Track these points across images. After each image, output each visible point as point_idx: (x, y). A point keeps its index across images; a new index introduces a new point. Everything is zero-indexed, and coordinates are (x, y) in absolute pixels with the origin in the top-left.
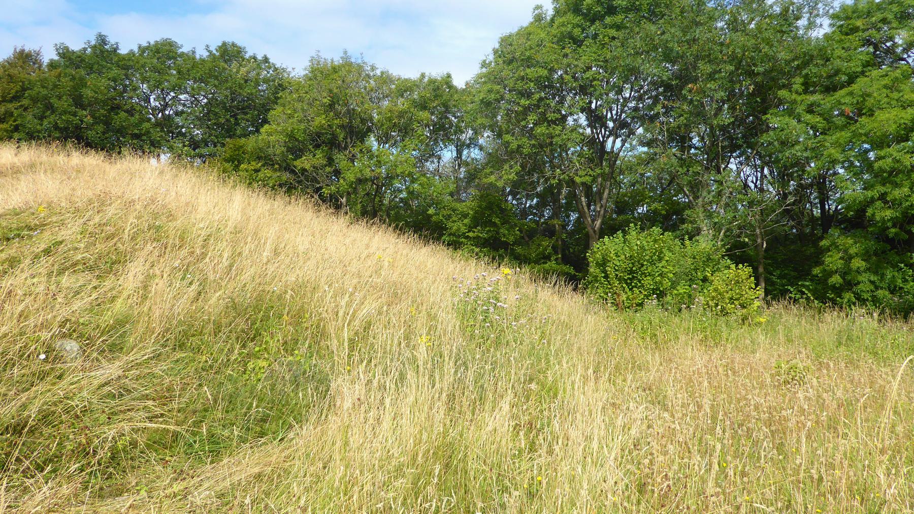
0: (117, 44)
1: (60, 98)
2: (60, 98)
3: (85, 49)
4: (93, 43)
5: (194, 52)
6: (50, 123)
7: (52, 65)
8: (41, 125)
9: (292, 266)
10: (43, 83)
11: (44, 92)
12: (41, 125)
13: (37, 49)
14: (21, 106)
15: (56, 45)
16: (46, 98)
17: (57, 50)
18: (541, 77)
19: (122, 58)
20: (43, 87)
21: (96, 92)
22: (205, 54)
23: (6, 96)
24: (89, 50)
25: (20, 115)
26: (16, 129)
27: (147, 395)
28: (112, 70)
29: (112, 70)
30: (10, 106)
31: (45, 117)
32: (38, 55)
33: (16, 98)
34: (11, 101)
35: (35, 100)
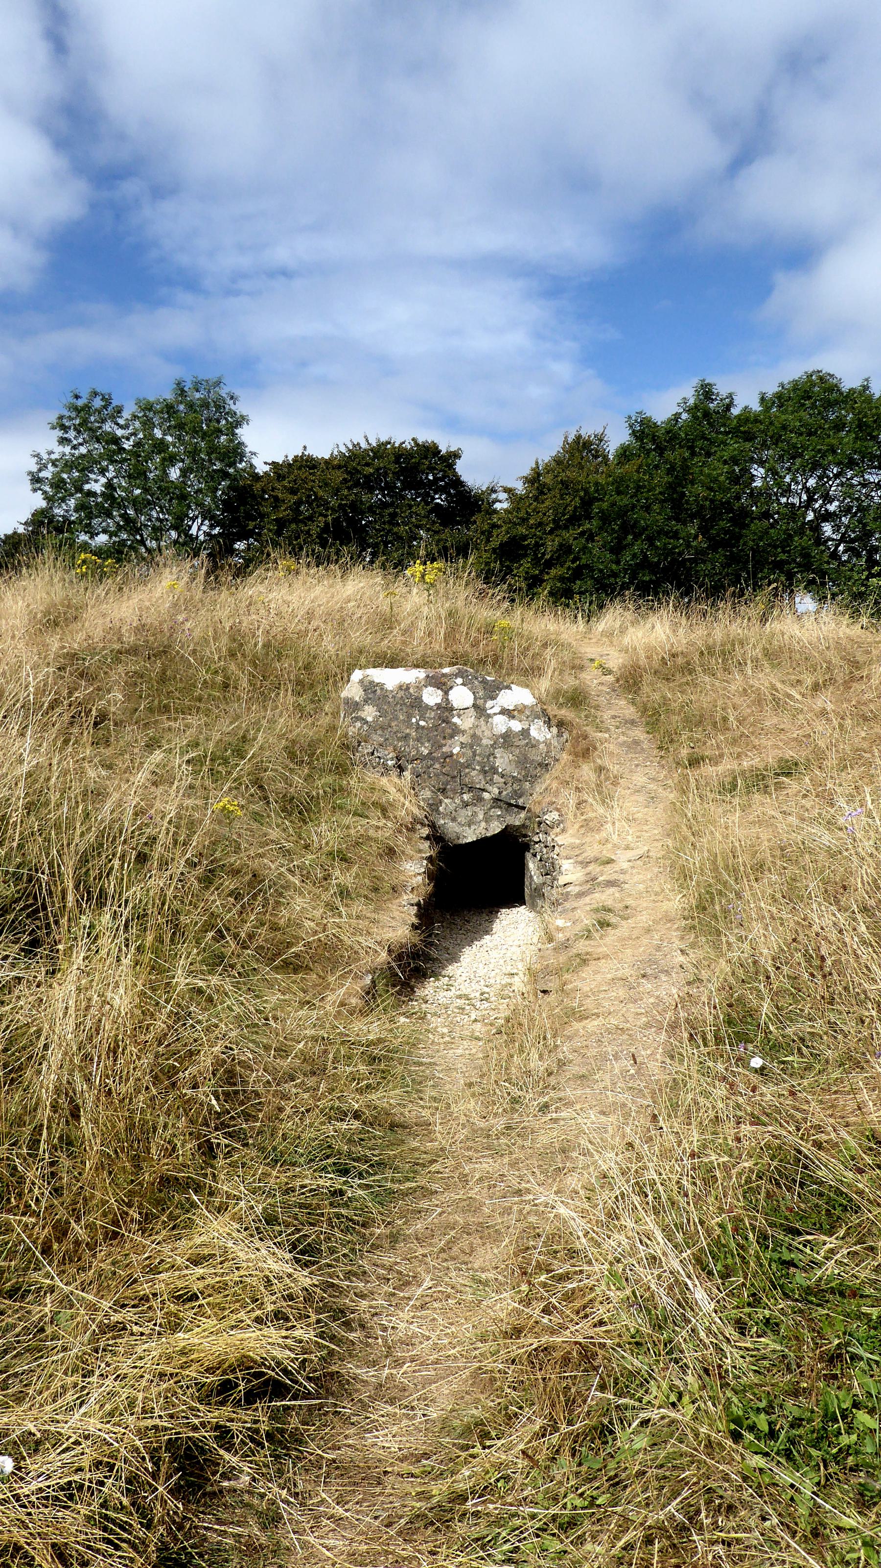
0: (730, 396)
1: (647, 508)
2: (647, 508)
3: (677, 416)
4: (692, 401)
5: (866, 388)
6: (634, 556)
7: (624, 454)
8: (618, 563)
9: (782, 1182)
10: (620, 487)
11: (623, 501)
12: (618, 563)
13: (600, 431)
14: (582, 534)
15: (630, 417)
16: (623, 513)
17: (631, 426)
18: (805, 849)
19: (746, 417)
20: (619, 493)
21: (711, 489)
22: (267, 468)
23: (559, 519)
24: (685, 416)
25: (584, 549)
26: (577, 574)
27: (851, 1200)
28: (726, 444)
29: (726, 444)
30: (568, 535)
31: (624, 547)
32: (601, 440)
33: (574, 520)
34: (566, 527)
35: (605, 518)
